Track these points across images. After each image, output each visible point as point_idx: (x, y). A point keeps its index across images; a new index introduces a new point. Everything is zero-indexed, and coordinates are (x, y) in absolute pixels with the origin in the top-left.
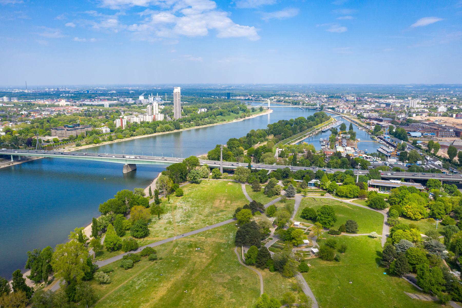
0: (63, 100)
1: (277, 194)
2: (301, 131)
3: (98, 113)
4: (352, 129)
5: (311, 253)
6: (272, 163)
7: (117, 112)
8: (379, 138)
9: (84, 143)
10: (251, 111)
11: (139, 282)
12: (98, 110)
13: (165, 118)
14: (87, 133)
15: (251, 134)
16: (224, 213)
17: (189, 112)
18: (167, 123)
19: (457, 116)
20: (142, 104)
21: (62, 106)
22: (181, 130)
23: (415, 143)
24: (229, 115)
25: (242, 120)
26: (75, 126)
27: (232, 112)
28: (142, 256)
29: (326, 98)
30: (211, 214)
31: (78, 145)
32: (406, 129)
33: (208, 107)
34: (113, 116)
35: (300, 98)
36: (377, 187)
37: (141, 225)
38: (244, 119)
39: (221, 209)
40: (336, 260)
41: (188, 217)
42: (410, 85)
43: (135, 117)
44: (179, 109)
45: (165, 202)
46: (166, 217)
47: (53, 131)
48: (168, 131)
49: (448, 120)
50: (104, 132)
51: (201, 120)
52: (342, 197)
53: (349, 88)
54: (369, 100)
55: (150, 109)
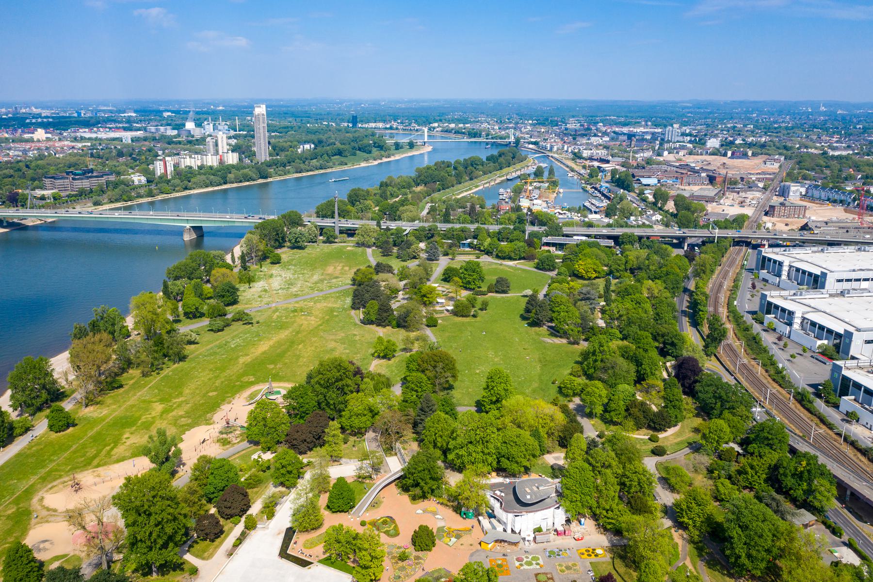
0: (39, 130)
1: (415, 257)
2: (471, 179)
3: (114, 153)
4: (554, 174)
5: (445, 312)
6: (413, 220)
9: (106, 201)
10: (394, 147)
11: (234, 342)
12: (113, 147)
13: (240, 159)
14: (108, 183)
15: (386, 183)
17: (283, 150)
18: (244, 168)
19: (733, 154)
20: (193, 136)
21: (39, 141)
22: (269, 180)
24: (355, 154)
25: (376, 163)
26: (87, 173)
27: (360, 149)
28: (233, 321)
29: (531, 125)
31: (96, 204)
33: (316, 141)
34: (146, 158)
36: (554, 245)
38: (380, 161)
39: (336, 275)
40: (474, 316)
41: (289, 284)
42: (687, 102)
43: (188, 157)
44: (265, 144)
45: (255, 270)
46: (258, 286)
47: (47, 182)
48: (248, 181)
49: (714, 160)
50: (136, 183)
51: (304, 162)
52: (504, 258)
53: (579, 107)
55: (211, 144)
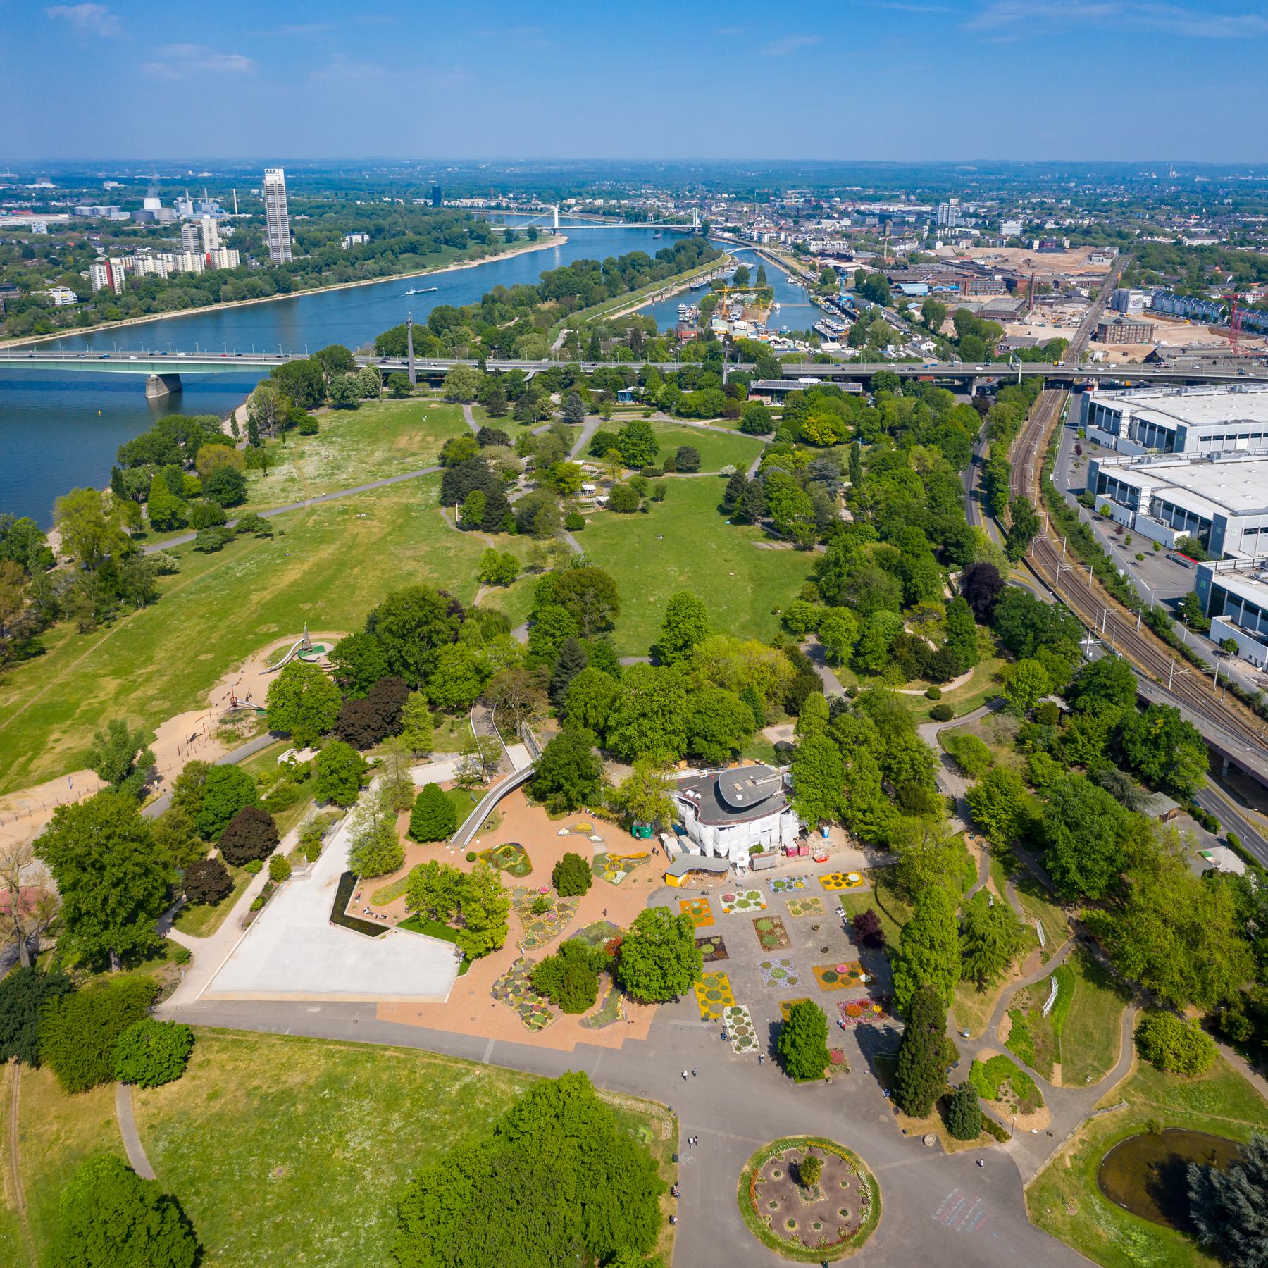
1: (543, 418)
2: (632, 289)
6: (540, 358)
7: (82, 246)
8: (827, 300)
10: (503, 239)
13: (243, 261)
16: (419, 457)
17: (315, 243)
18: (250, 275)
19: (1041, 245)
22: (294, 294)
23: (903, 308)
24: (438, 251)
27: (446, 242)
28: (239, 532)
29: (726, 200)
30: (389, 460)
32: (894, 274)
34: (75, 260)
35: (651, 202)
36: (768, 392)
37: (227, 477)
38: (481, 262)
40: (644, 511)
41: (333, 468)
45: (274, 447)
49: (1014, 255)
50: (59, 302)
51: (353, 265)
52: (689, 416)
54: (842, 207)
55: (190, 235)
